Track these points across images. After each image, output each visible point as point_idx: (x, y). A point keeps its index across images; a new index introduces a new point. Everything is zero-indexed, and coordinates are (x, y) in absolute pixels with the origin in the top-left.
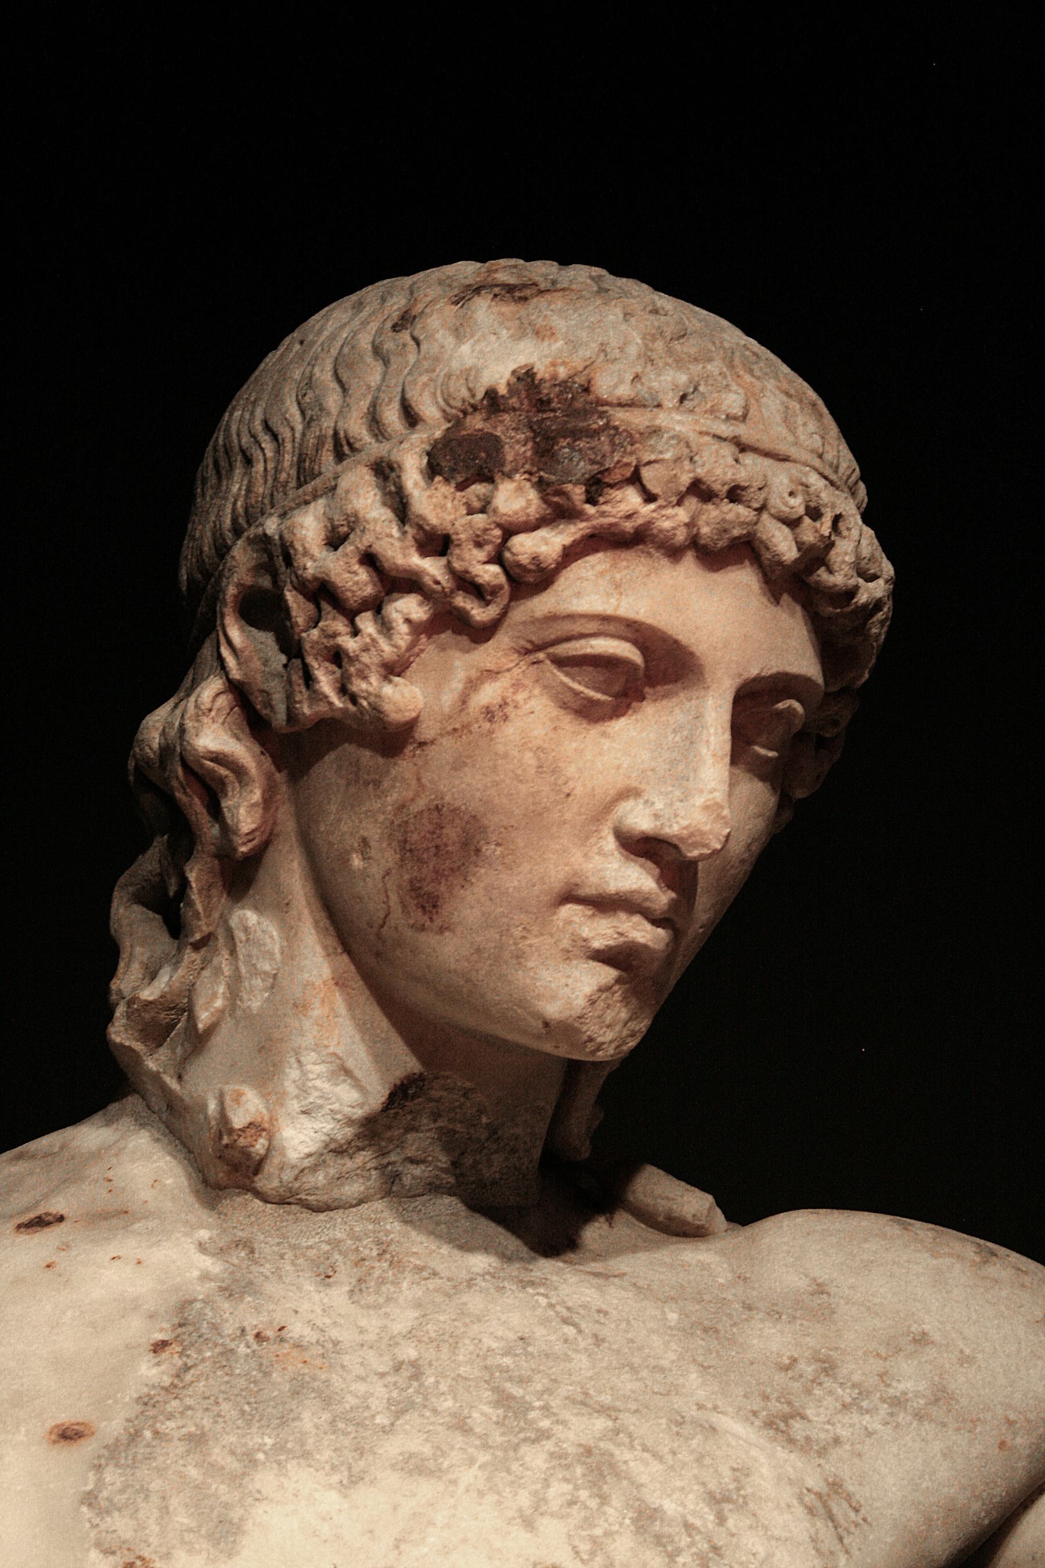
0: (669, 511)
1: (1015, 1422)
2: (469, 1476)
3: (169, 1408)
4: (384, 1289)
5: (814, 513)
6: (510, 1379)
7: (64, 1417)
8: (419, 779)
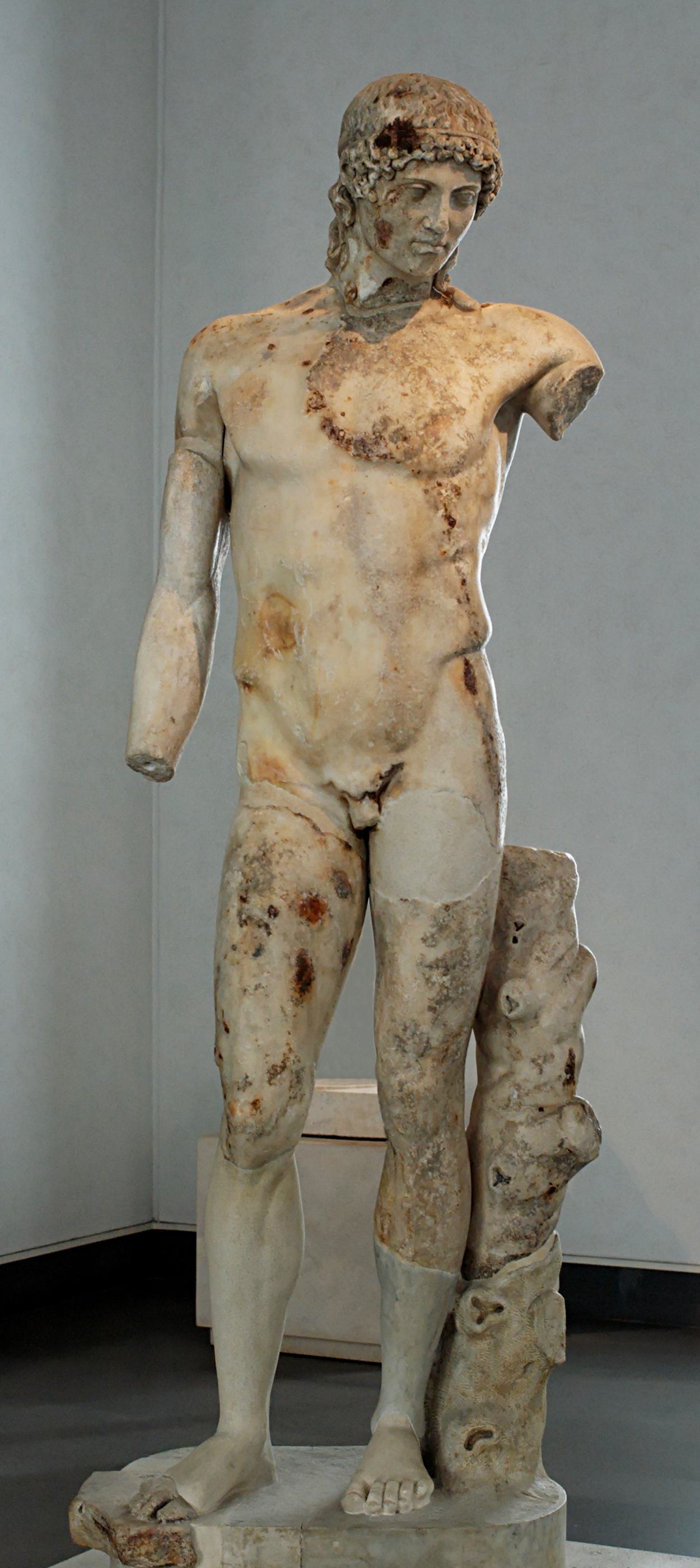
2: (391, 374)
5: (468, 148)
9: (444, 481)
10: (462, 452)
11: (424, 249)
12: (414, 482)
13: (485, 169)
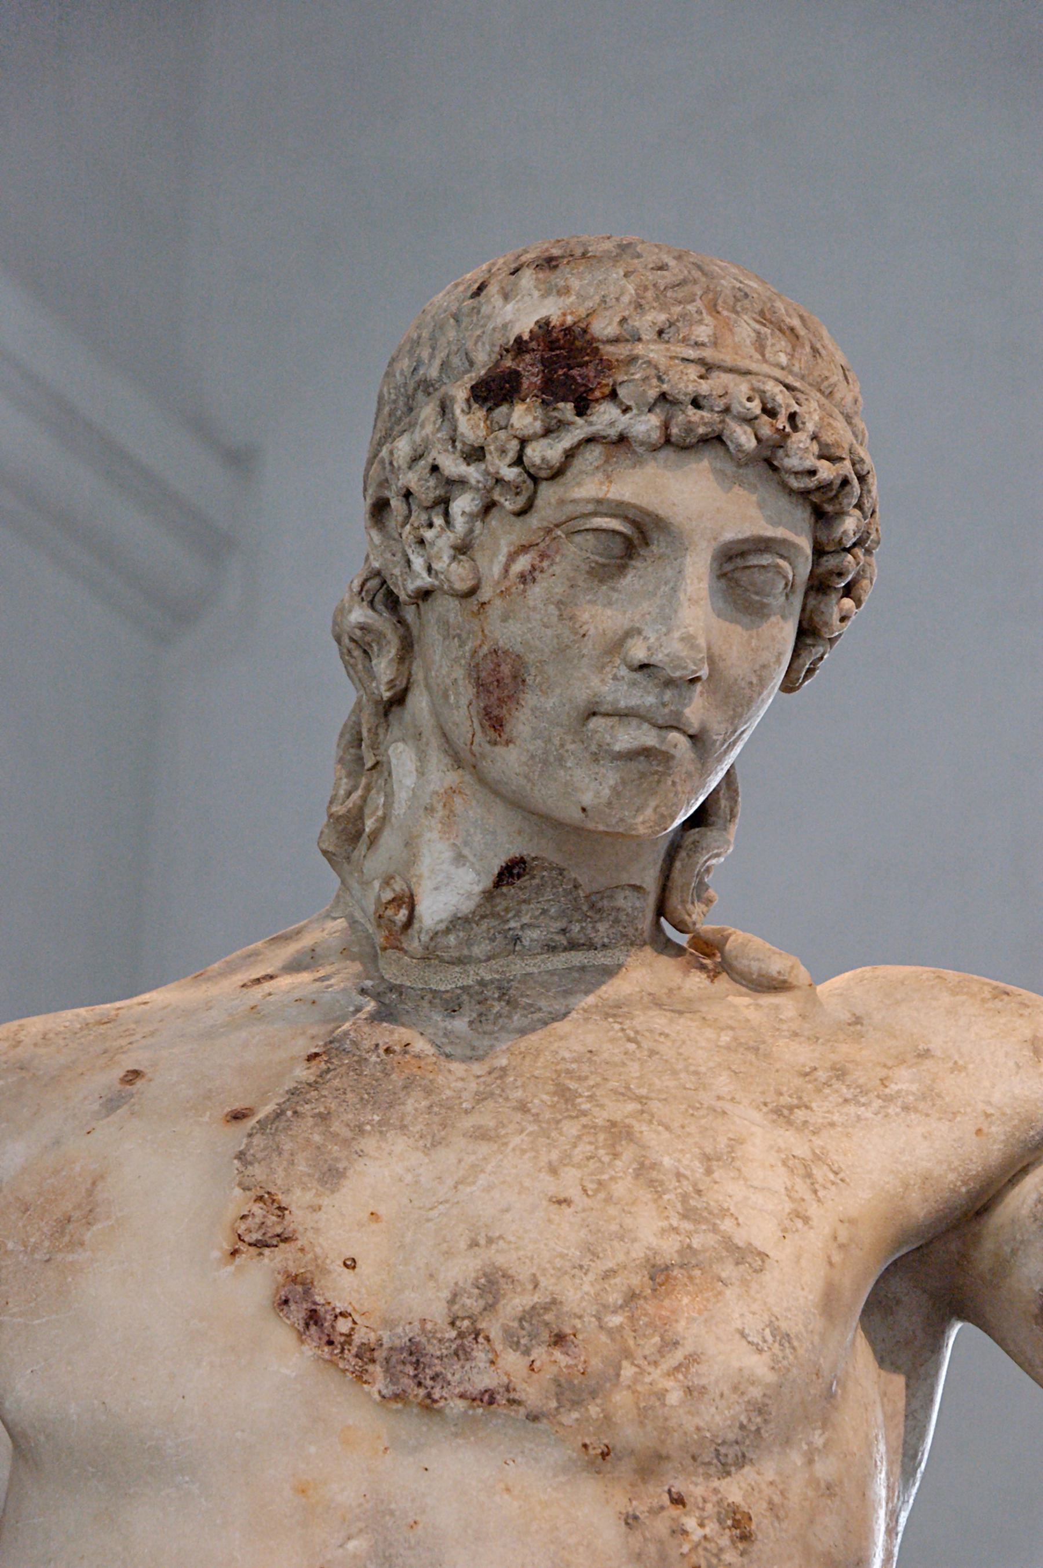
0: (643, 418)
1: (992, 1115)
3: (308, 1096)
4: (500, 1020)
5: (770, 412)
6: (571, 1078)
7: (237, 1105)
8: (483, 631)
9: (695, 1489)
10: (755, 1393)
11: (628, 737)
12: (590, 1488)
13: (824, 487)
